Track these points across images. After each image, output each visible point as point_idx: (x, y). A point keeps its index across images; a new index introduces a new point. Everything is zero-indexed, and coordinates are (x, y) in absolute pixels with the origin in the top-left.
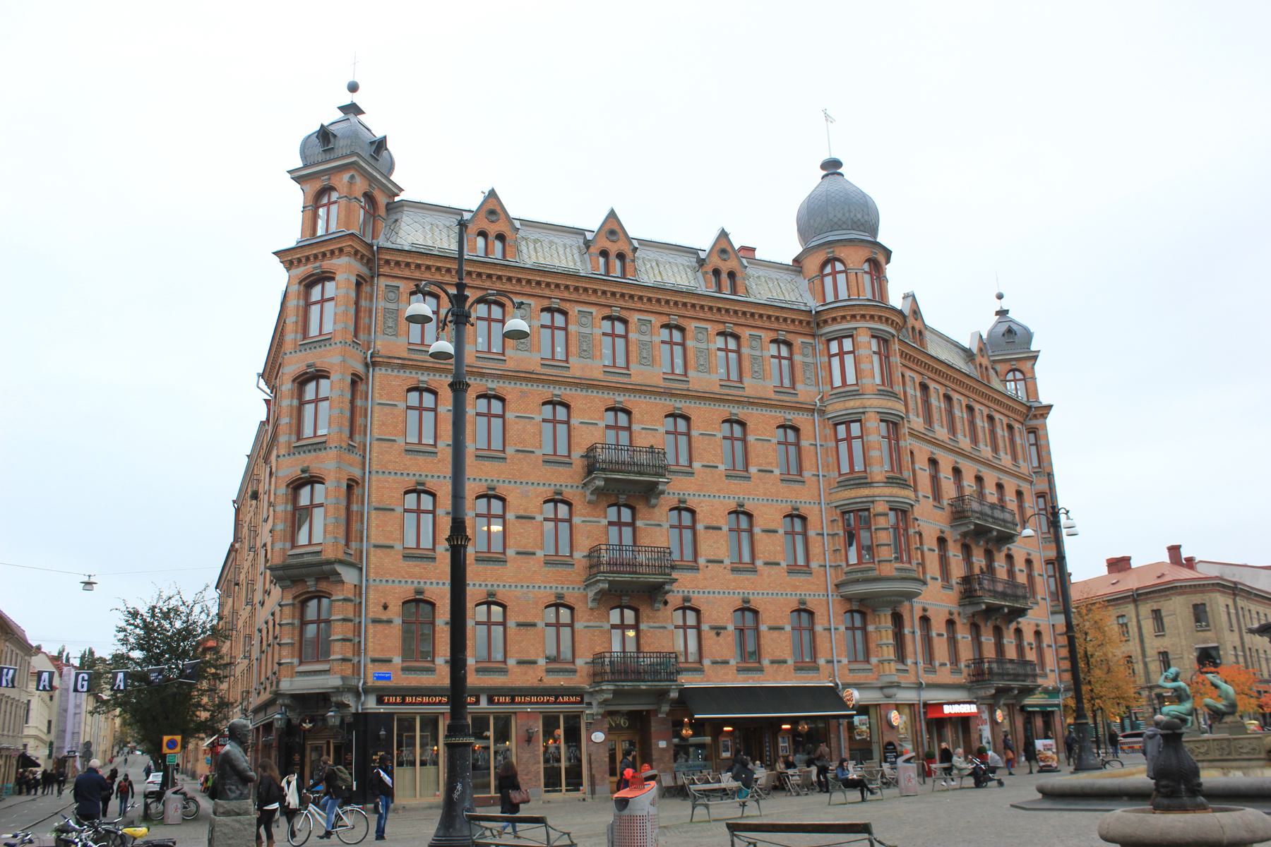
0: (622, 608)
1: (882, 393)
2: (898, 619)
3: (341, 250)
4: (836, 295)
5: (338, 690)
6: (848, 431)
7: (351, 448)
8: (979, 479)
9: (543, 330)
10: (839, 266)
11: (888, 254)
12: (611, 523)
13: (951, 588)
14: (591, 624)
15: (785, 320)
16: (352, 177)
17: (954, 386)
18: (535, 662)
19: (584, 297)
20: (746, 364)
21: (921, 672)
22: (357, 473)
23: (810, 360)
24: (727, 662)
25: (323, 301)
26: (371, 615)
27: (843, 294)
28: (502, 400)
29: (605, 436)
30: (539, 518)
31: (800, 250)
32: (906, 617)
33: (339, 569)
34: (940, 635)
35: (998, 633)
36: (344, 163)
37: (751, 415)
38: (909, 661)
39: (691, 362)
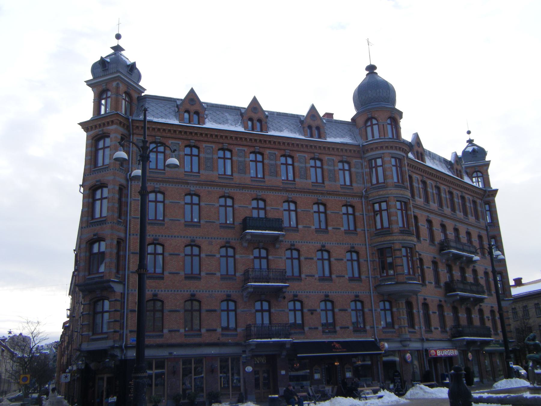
0: (261, 301)
1: (397, 186)
2: (409, 305)
3: (112, 122)
4: (373, 137)
5: (113, 347)
6: (380, 206)
7: (119, 223)
8: (456, 230)
9: (219, 160)
10: (374, 122)
11: (400, 114)
12: (255, 258)
13: (440, 287)
14: (245, 309)
15: (346, 150)
16: (118, 84)
17: (441, 181)
18: (215, 330)
19: (240, 142)
20: (326, 174)
21: (423, 333)
22: (122, 235)
23: (360, 171)
24: (317, 328)
25: (104, 148)
26: (130, 308)
27: (377, 135)
28: (198, 196)
29: (252, 212)
30: (218, 256)
31: (356, 113)
32: (414, 303)
33: (112, 285)
34: (434, 313)
35: (469, 312)
36: (114, 77)
37: (329, 200)
38: (417, 327)
39: (297, 174)
